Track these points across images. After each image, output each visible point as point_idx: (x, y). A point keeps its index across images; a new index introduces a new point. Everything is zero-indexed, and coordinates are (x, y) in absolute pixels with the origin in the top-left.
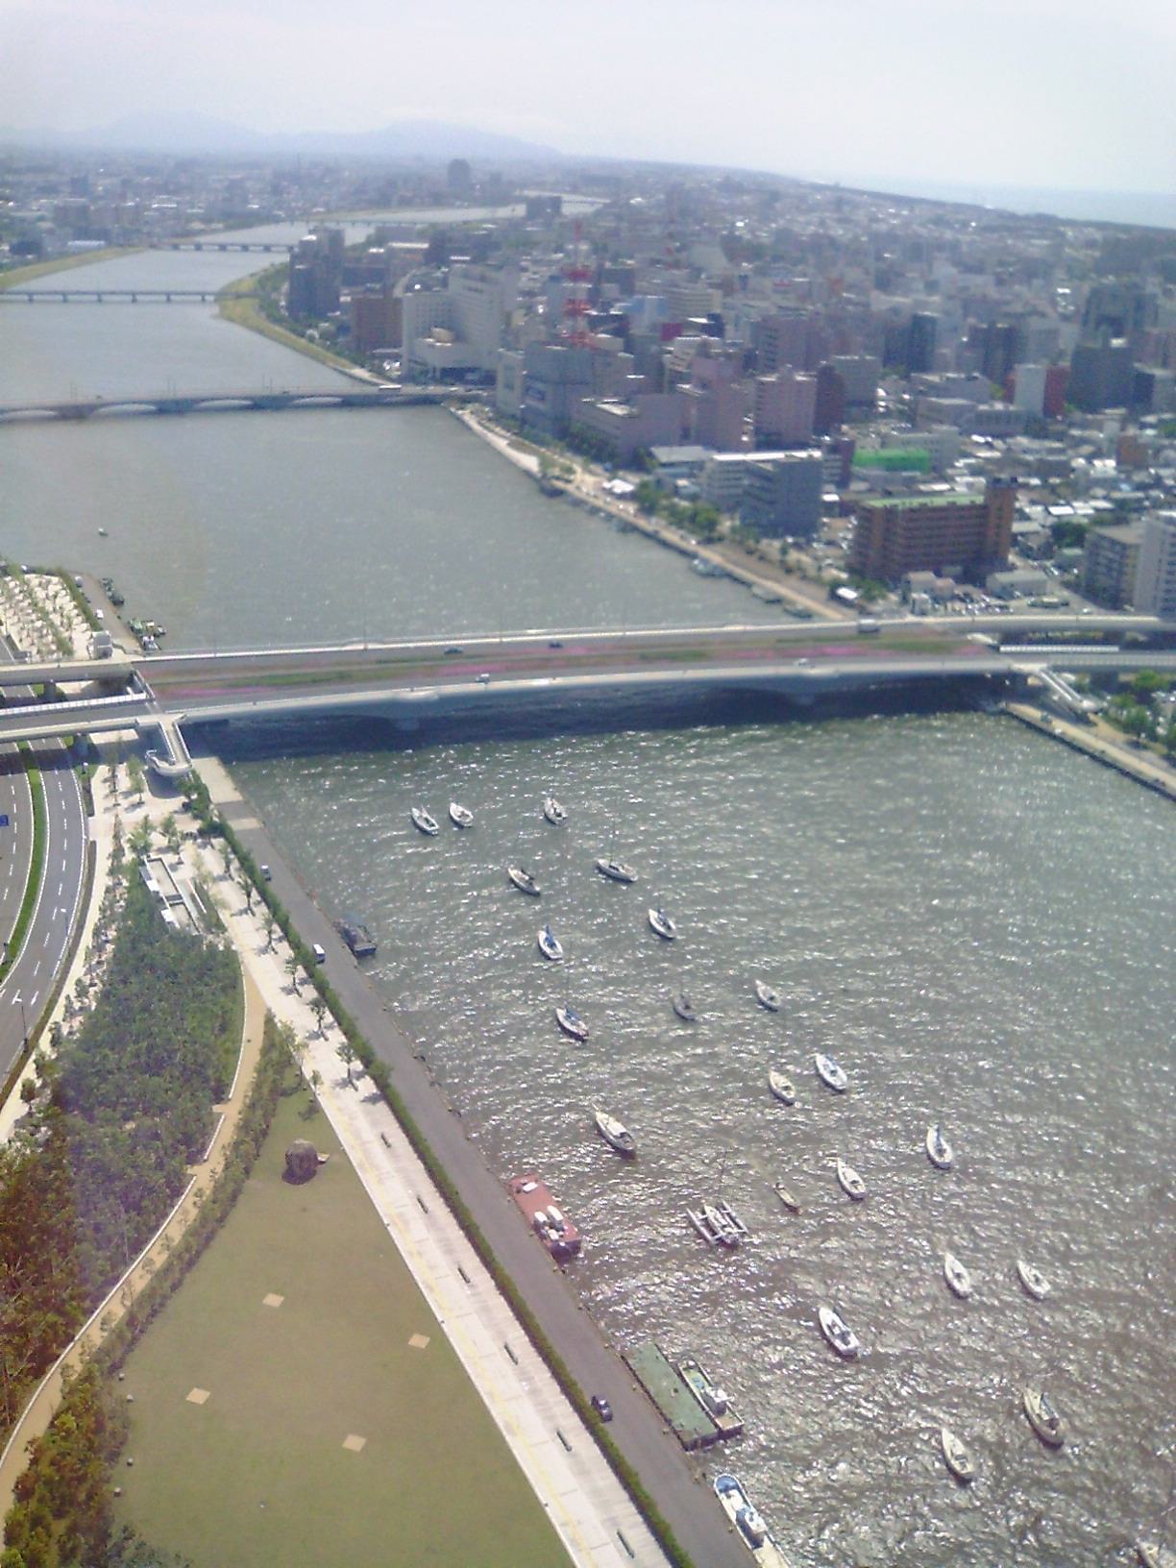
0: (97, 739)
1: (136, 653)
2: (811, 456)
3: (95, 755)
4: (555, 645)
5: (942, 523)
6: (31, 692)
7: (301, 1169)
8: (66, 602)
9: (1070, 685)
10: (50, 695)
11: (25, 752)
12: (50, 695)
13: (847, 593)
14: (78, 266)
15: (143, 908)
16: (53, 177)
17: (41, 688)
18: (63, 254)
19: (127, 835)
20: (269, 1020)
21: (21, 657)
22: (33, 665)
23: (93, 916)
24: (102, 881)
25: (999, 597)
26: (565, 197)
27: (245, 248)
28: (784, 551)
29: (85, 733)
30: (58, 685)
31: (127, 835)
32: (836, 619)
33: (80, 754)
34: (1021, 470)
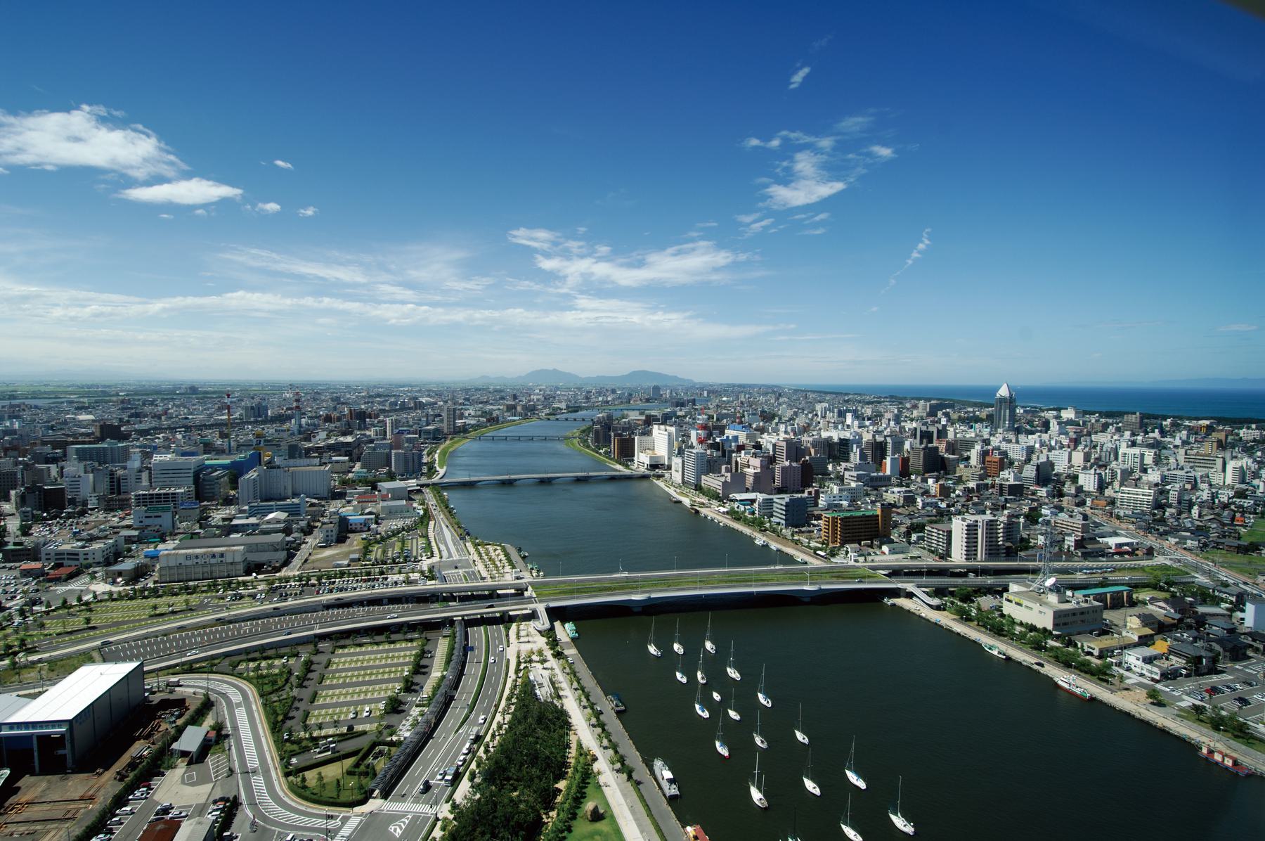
3: (512, 619)
4: (275, 609)
7: (597, 816)
8: (502, 557)
11: (482, 617)
15: (527, 690)
16: (503, 394)
19: (523, 656)
20: (580, 746)
21: (483, 579)
22: (489, 582)
23: (507, 692)
25: (902, 553)
28: (793, 535)
29: (508, 611)
31: (523, 656)
32: (815, 563)
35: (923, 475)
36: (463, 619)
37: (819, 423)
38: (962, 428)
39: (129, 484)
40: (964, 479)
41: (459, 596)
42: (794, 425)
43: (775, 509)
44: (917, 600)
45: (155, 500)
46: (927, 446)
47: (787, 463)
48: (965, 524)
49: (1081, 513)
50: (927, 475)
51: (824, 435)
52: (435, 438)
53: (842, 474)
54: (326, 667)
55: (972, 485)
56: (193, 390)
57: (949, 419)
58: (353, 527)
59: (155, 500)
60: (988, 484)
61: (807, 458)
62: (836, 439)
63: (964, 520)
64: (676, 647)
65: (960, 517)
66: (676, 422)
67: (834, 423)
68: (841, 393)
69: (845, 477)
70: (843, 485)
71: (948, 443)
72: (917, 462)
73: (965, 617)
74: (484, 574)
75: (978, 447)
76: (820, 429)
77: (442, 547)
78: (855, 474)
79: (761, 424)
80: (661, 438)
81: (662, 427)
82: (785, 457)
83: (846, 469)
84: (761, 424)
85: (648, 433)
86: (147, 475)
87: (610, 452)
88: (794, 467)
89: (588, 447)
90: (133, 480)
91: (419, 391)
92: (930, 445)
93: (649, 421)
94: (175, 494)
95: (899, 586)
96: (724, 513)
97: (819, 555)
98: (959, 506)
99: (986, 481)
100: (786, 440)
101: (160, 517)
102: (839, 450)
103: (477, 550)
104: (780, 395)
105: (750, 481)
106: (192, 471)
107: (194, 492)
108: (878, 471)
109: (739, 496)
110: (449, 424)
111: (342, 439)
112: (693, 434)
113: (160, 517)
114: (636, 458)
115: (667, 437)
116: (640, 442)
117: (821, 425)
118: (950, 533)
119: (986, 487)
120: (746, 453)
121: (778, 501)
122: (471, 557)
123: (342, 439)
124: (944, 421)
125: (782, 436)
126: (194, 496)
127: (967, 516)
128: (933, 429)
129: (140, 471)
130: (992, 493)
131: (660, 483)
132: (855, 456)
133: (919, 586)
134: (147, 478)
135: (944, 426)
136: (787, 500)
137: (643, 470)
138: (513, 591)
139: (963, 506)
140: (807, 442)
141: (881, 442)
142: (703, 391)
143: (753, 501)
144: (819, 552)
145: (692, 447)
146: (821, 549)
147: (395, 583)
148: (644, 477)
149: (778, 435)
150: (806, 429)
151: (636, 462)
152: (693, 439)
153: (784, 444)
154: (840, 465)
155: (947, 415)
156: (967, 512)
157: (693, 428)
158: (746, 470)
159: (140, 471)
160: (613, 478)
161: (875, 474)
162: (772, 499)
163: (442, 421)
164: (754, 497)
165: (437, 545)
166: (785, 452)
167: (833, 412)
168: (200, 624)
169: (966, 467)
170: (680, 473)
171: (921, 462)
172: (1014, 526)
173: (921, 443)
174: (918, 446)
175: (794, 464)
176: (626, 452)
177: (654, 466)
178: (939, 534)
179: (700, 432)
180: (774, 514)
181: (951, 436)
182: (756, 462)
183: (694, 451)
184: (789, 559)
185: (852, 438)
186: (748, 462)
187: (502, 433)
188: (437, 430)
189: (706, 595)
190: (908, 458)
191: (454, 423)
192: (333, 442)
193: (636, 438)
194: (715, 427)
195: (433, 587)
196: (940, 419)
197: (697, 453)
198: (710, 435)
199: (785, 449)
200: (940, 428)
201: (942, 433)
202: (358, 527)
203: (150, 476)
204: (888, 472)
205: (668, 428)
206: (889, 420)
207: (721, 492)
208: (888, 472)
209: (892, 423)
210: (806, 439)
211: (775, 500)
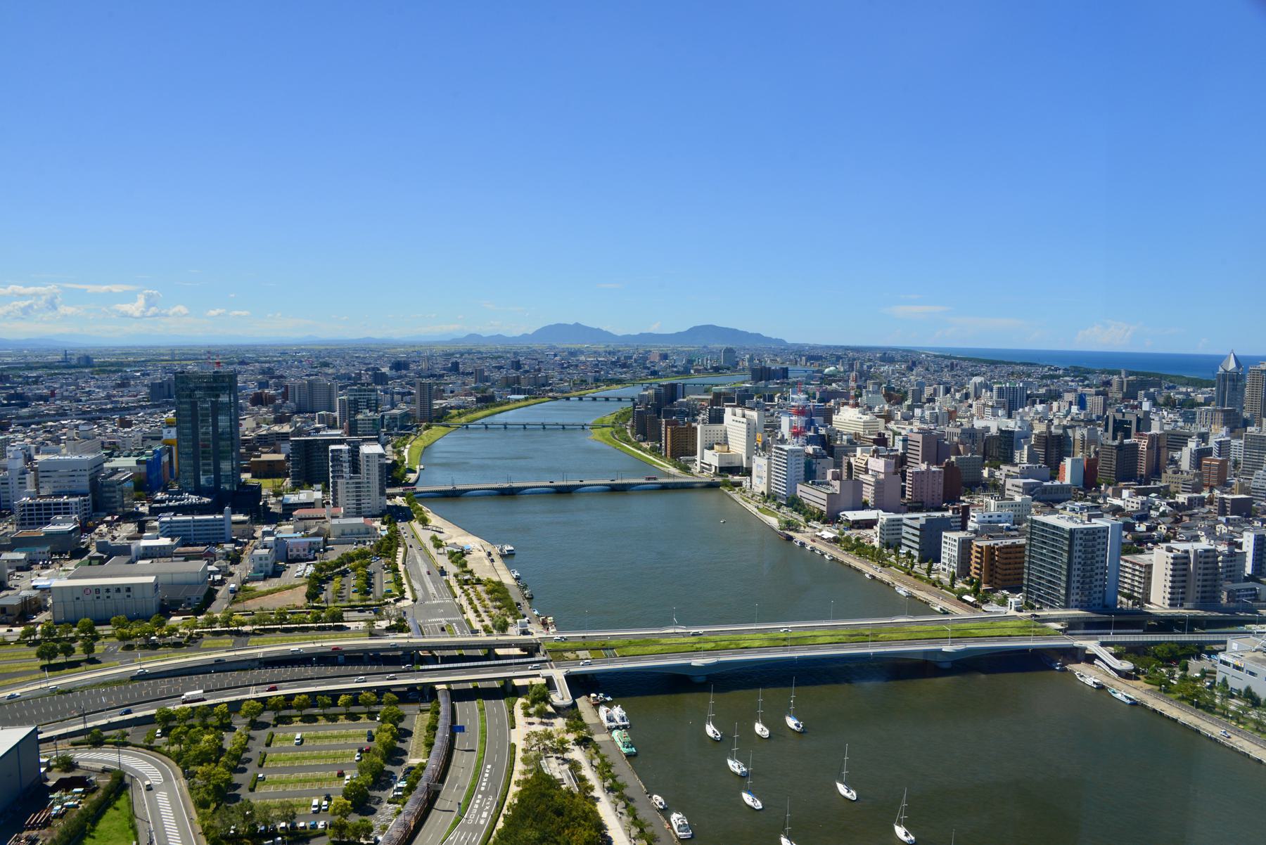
0: (517, 682)
1: (541, 632)
2: (943, 516)
5: (1229, 564)
6: (480, 652)
9: (1111, 654)
10: (491, 655)
12: (491, 655)
13: (971, 599)
14: (159, 347)
17: (486, 651)
18: (508, 402)
21: (474, 632)
24: (519, 766)
26: (790, 368)
27: (607, 399)
29: (511, 678)
30: (496, 650)
32: (960, 612)
33: (508, 691)
34: (1234, 546)
35: (1116, 484)
36: (449, 689)
37: (971, 406)
38: (1171, 416)
39: (11, 490)
40: (1172, 489)
41: (442, 657)
42: (934, 409)
43: (904, 535)
44: (1100, 663)
45: (43, 512)
46: (1122, 443)
47: (924, 467)
48: (1171, 555)
49: (692, 474)
50: (1122, 484)
51: (978, 424)
52: (403, 427)
53: (1002, 482)
54: (268, 745)
55: (1182, 498)
56: (87, 361)
57: (1155, 404)
58: (295, 553)
59: (43, 512)
60: (1204, 498)
61: (953, 458)
62: (994, 431)
63: (1170, 550)
64: (759, 728)
65: (1164, 545)
66: (758, 403)
67: (992, 407)
68: (1003, 363)
69: (1007, 487)
70: (1003, 499)
71: (1152, 438)
72: (1106, 467)
73: (1165, 688)
74: (477, 626)
75: (1192, 445)
76: (972, 416)
77: (417, 586)
78: (1021, 482)
79: (886, 407)
80: (736, 423)
81: (739, 411)
82: (920, 457)
83: (1007, 476)
84: (886, 407)
85: (717, 418)
86: (33, 478)
87: (660, 448)
88: (934, 472)
89: (628, 441)
90: (16, 481)
91: (380, 358)
92: (1126, 441)
93: (720, 399)
94: (67, 504)
95: (1077, 643)
96: (829, 540)
97: (965, 601)
98: (1162, 529)
99: (1203, 494)
100: (921, 431)
101: (1013, 485)
102: (1004, 446)
103: (464, 591)
104: (914, 364)
105: (868, 494)
106: (88, 473)
107: (90, 502)
108: (1053, 478)
109: (852, 516)
110: (422, 408)
111: (276, 428)
112: (785, 422)
113: (1013, 485)
114: (698, 458)
115: (745, 426)
116: (705, 433)
117: (974, 410)
118: (1149, 567)
119: (1202, 502)
120: (863, 452)
121: (908, 522)
122: (457, 600)
123: (276, 428)
124: (1146, 406)
125: (917, 425)
126: (91, 506)
127: (1173, 544)
128: (1131, 417)
129: (24, 473)
130: (1210, 512)
131: (736, 495)
132: (1022, 456)
133: (1103, 644)
134: (33, 483)
135: (1147, 413)
136: (923, 521)
137: (707, 477)
138: (517, 651)
139: (1169, 529)
140: (954, 434)
141: (1059, 436)
142: (800, 356)
143: (869, 524)
144: (966, 597)
145: (783, 441)
146: (968, 593)
147: (355, 635)
148: (712, 486)
149: (911, 424)
150: (952, 415)
151: (698, 463)
152: (785, 430)
153: (919, 438)
154: (1000, 469)
155: (1151, 398)
156: (1175, 538)
157: (785, 413)
158: (862, 477)
159: (24, 473)
160: (665, 487)
161: (1050, 483)
162: (900, 520)
163: (412, 402)
164: (874, 517)
165: (409, 582)
166: (920, 449)
167: (991, 390)
168: (101, 681)
169: (1175, 473)
170: (765, 480)
171: (1114, 467)
172: (1237, 558)
173: (1114, 438)
174: (1110, 442)
175: (934, 468)
176: (683, 449)
177: (725, 470)
178: (1135, 570)
179: (794, 418)
180: (904, 541)
181: (1155, 430)
182: (878, 465)
183: (786, 447)
184: (925, 608)
185: (1017, 429)
186: (866, 464)
187: (500, 418)
188: (406, 416)
189: (799, 658)
190: (1096, 460)
191: (431, 405)
192: (264, 433)
193: (699, 427)
194: (819, 412)
195: (406, 641)
196: (1141, 403)
197: (791, 450)
198: (810, 424)
199: (920, 445)
200: (1141, 415)
201: (1144, 423)
202: (302, 553)
203: (36, 480)
204: (1067, 481)
205: (747, 412)
206: (1071, 404)
207: (824, 509)
208: (1067, 481)
209: (1075, 409)
210: (951, 431)
211: (905, 521)
